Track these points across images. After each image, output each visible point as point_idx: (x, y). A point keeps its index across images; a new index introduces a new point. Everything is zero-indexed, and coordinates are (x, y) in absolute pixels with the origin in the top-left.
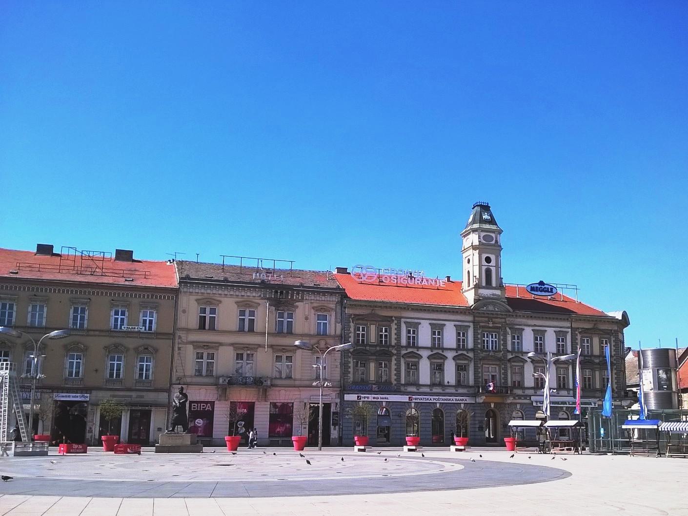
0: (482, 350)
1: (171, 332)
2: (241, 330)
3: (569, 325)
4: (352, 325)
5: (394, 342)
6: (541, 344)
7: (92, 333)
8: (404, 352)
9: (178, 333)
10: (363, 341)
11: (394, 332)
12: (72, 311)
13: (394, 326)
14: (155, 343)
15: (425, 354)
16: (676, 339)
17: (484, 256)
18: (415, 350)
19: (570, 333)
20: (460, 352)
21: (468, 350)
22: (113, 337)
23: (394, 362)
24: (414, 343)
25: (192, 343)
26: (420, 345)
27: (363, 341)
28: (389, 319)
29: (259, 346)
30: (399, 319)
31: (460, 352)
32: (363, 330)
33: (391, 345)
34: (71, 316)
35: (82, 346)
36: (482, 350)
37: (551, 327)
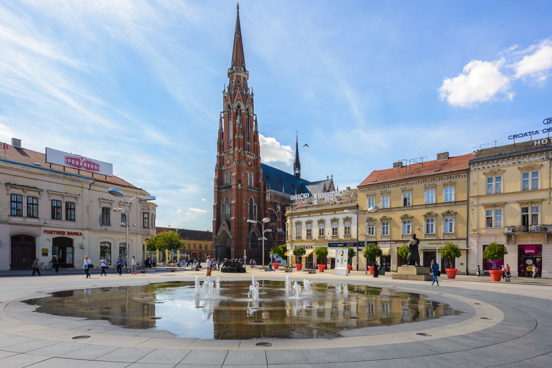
1: (466, 199)
2: (525, 190)
7: (415, 207)
9: (471, 199)
14: (455, 209)
16: (74, 338)
22: (427, 208)
25: (483, 205)
29: (543, 200)
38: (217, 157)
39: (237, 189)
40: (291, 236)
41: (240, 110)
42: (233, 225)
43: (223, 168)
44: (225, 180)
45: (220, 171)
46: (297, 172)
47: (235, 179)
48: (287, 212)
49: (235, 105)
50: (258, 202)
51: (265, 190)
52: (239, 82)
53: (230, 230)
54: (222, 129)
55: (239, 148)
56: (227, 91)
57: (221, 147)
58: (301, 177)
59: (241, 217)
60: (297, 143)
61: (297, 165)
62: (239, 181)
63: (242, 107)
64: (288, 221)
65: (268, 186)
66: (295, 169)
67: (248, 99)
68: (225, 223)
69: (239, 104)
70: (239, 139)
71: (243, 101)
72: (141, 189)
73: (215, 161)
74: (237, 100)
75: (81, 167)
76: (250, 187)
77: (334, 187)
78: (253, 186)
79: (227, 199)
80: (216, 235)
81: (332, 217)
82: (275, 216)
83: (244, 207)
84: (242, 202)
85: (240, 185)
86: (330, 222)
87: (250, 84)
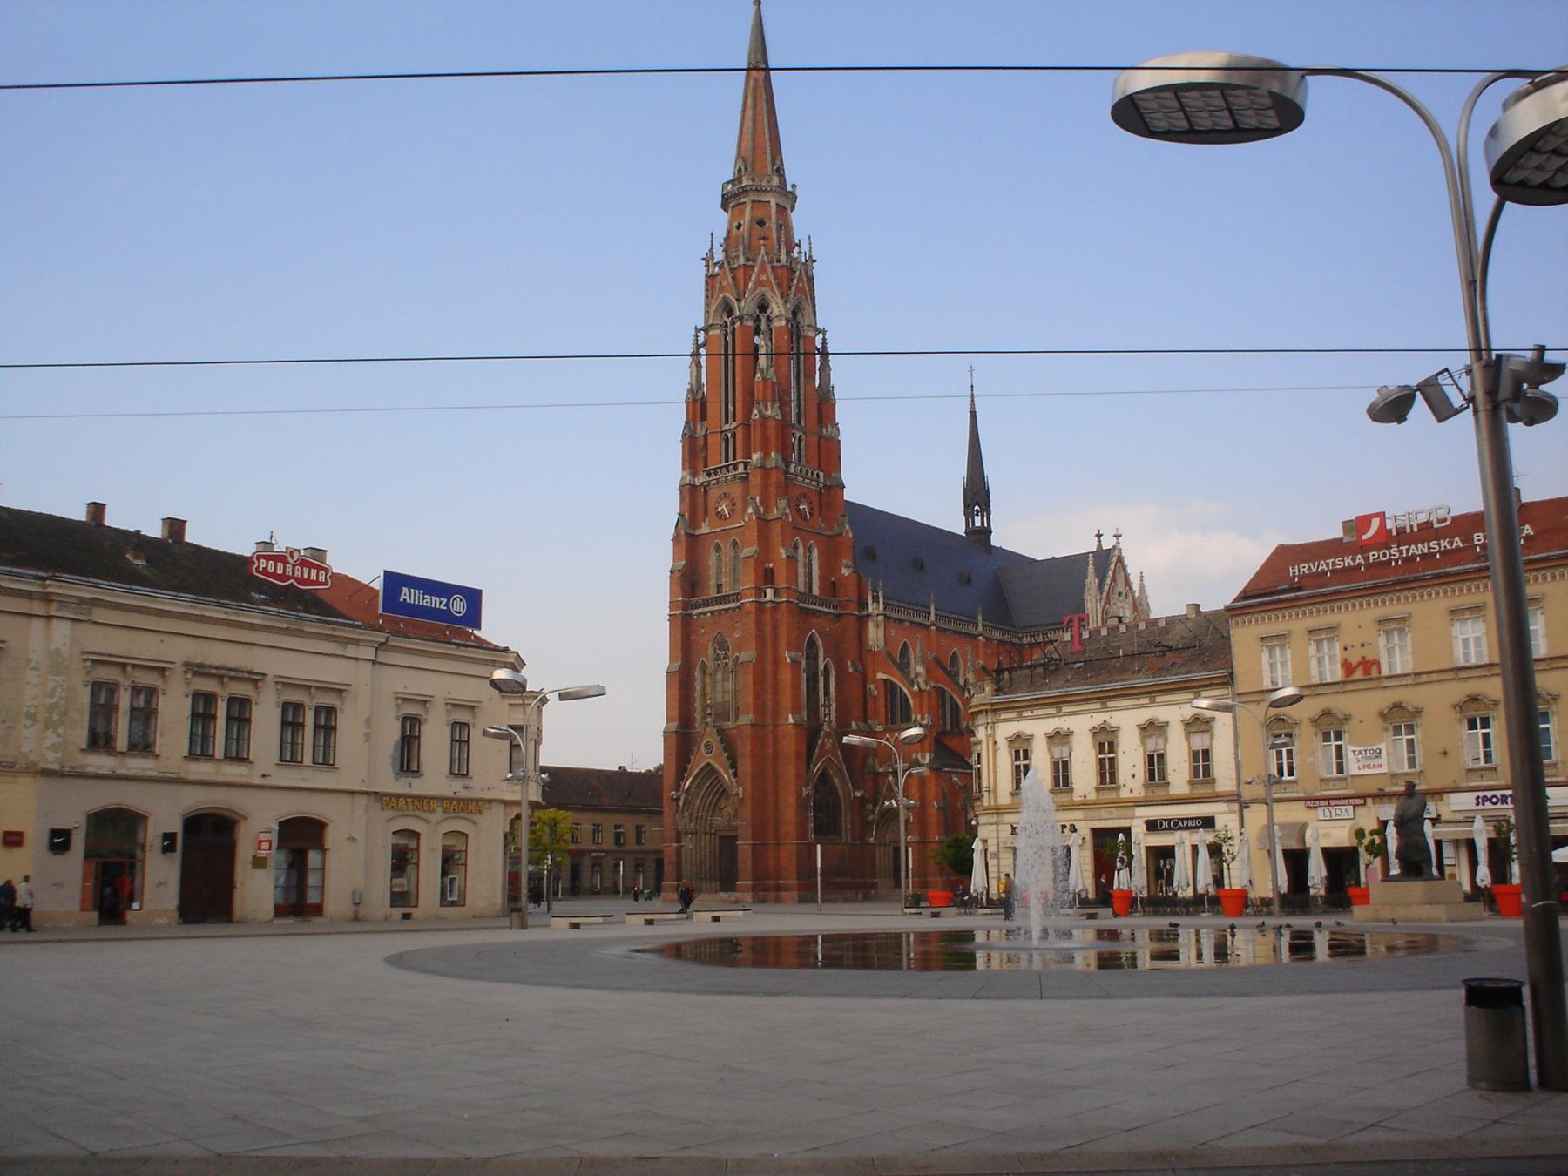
38: (682, 488)
39: (760, 606)
40: (993, 790)
41: (769, 320)
42: (745, 749)
43: (704, 529)
44: (712, 572)
45: (690, 542)
46: (978, 523)
47: (751, 570)
48: (975, 701)
49: (747, 306)
50: (836, 652)
51: (863, 605)
52: (761, 223)
53: (733, 766)
54: (700, 386)
55: (766, 455)
56: (719, 256)
57: (694, 451)
58: (995, 541)
59: (776, 711)
60: (973, 414)
61: (977, 495)
62: (768, 577)
63: (777, 308)
64: (981, 733)
65: (875, 590)
66: (969, 514)
67: (796, 280)
68: (712, 738)
69: (763, 297)
70: (764, 419)
71: (779, 285)
72: (506, 650)
73: (669, 508)
74: (759, 283)
75: (289, 578)
76: (807, 596)
77: (1127, 576)
78: (816, 591)
79: (722, 644)
80: (678, 788)
81: (1144, 715)
82: (905, 700)
83: (786, 676)
84: (777, 660)
85: (770, 593)
86: (1136, 732)
87: (802, 223)
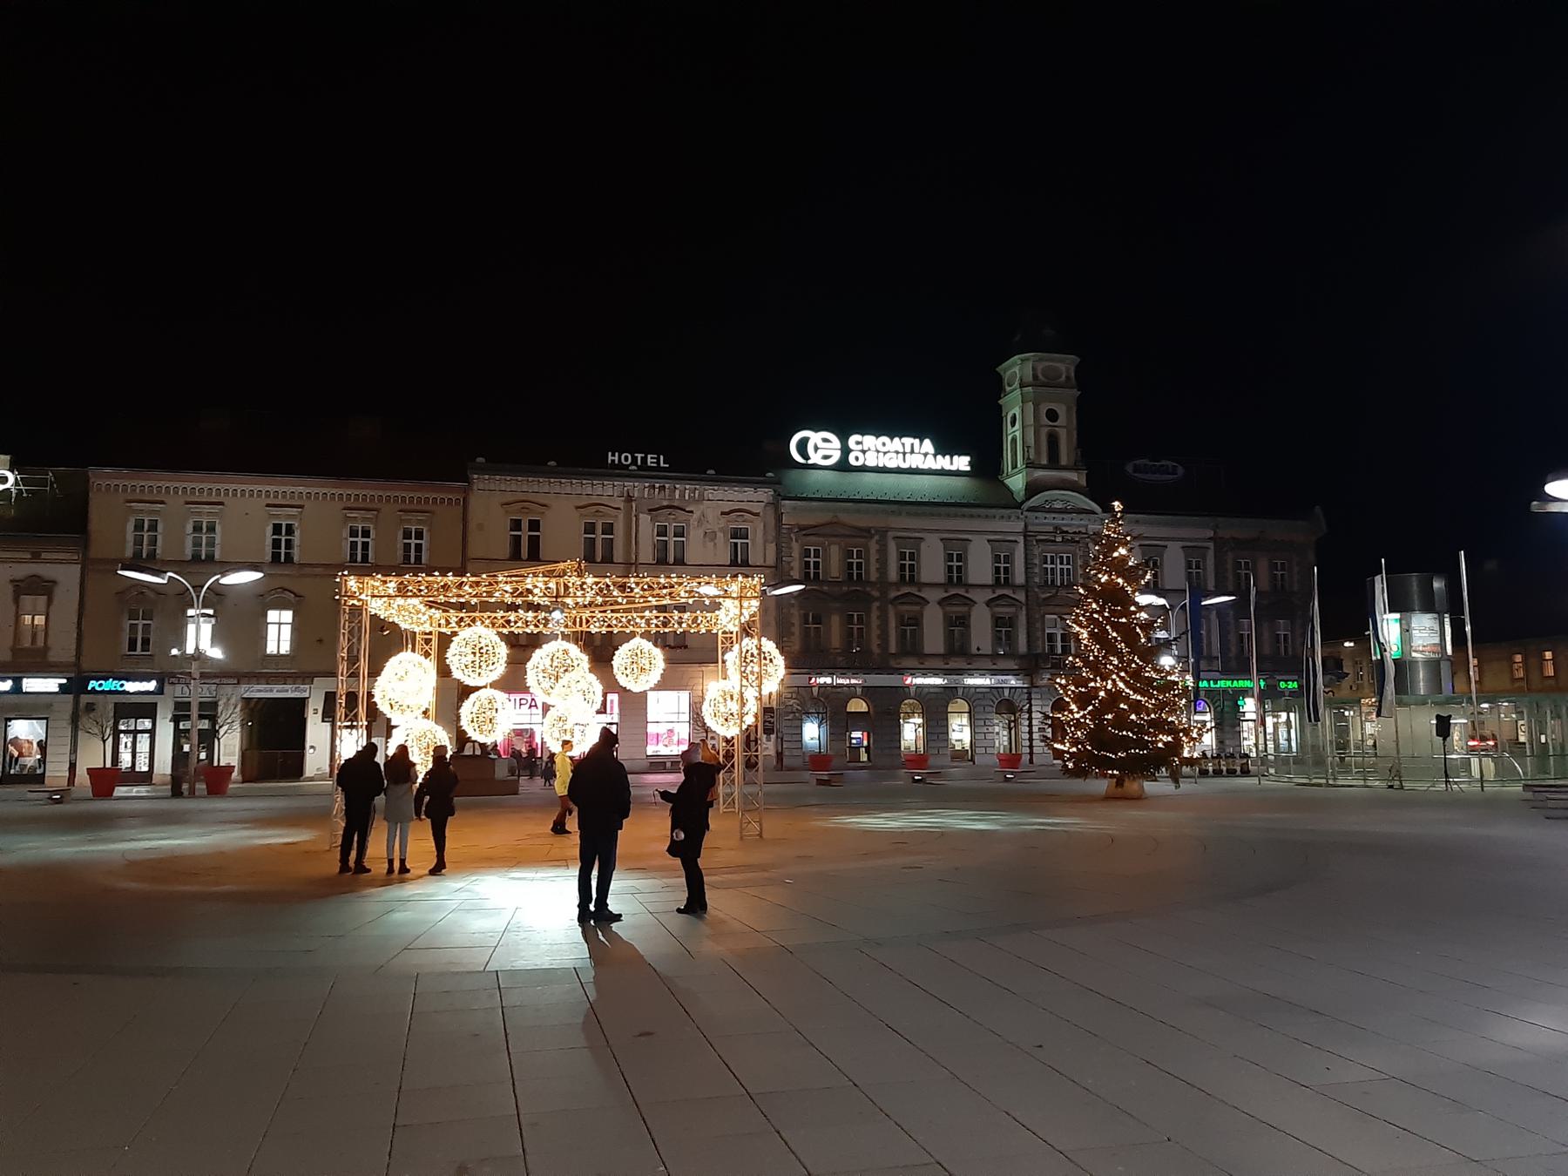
0: (1045, 585)
3: (1211, 534)
4: (795, 546)
5: (874, 576)
6: (959, 568)
7: (308, 570)
8: (893, 594)
10: (859, 575)
11: (874, 557)
12: (130, 526)
13: (873, 546)
15: (981, 597)
17: (1044, 409)
18: (914, 590)
19: (1022, 545)
20: (1000, 592)
21: (1015, 587)
23: (875, 614)
24: (912, 577)
26: (971, 581)
27: (859, 575)
28: (866, 532)
30: (883, 533)
31: (1000, 592)
32: (816, 556)
33: (869, 582)
34: (269, 542)
35: (1209, 740)
36: (1045, 585)
37: (1173, 539)
